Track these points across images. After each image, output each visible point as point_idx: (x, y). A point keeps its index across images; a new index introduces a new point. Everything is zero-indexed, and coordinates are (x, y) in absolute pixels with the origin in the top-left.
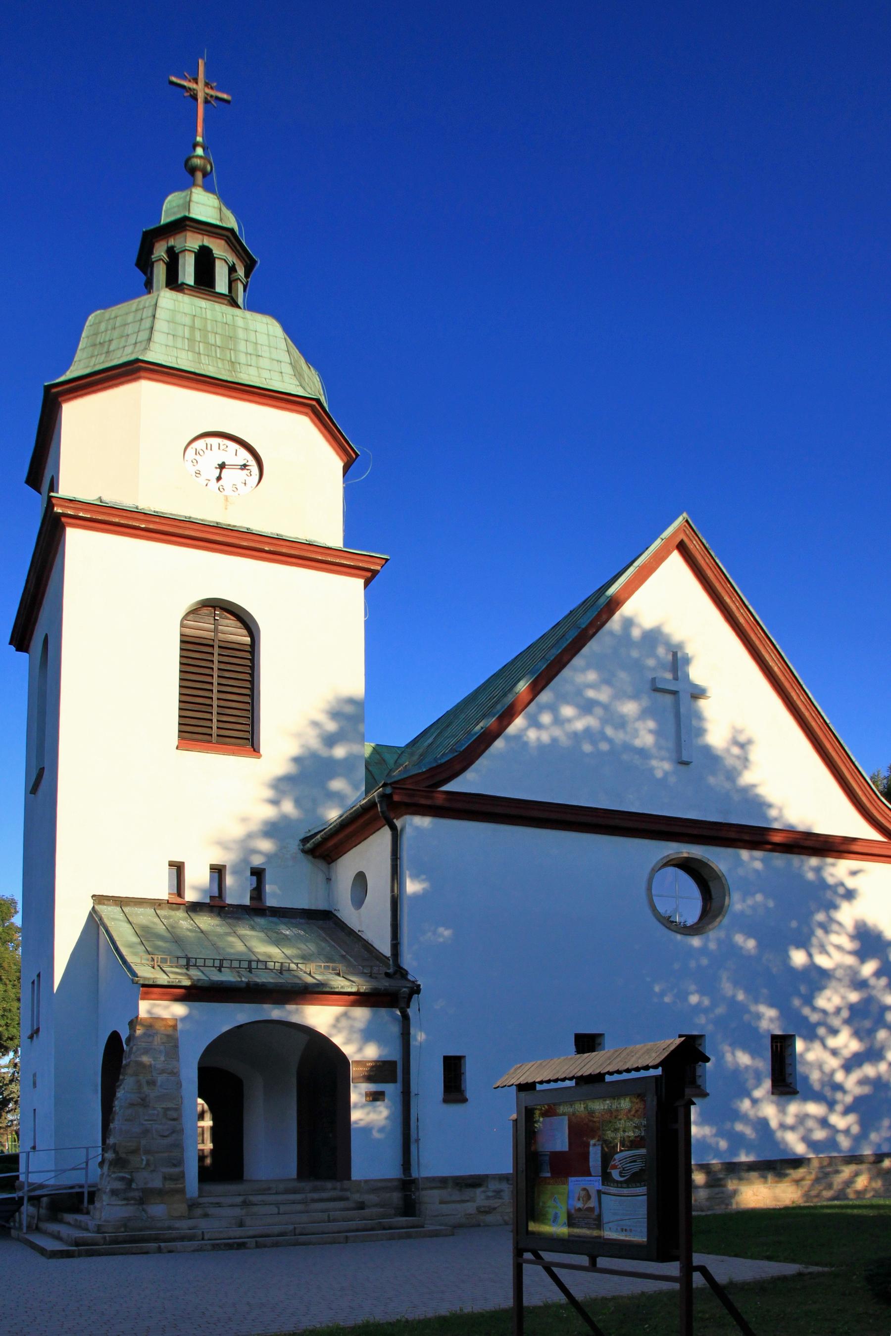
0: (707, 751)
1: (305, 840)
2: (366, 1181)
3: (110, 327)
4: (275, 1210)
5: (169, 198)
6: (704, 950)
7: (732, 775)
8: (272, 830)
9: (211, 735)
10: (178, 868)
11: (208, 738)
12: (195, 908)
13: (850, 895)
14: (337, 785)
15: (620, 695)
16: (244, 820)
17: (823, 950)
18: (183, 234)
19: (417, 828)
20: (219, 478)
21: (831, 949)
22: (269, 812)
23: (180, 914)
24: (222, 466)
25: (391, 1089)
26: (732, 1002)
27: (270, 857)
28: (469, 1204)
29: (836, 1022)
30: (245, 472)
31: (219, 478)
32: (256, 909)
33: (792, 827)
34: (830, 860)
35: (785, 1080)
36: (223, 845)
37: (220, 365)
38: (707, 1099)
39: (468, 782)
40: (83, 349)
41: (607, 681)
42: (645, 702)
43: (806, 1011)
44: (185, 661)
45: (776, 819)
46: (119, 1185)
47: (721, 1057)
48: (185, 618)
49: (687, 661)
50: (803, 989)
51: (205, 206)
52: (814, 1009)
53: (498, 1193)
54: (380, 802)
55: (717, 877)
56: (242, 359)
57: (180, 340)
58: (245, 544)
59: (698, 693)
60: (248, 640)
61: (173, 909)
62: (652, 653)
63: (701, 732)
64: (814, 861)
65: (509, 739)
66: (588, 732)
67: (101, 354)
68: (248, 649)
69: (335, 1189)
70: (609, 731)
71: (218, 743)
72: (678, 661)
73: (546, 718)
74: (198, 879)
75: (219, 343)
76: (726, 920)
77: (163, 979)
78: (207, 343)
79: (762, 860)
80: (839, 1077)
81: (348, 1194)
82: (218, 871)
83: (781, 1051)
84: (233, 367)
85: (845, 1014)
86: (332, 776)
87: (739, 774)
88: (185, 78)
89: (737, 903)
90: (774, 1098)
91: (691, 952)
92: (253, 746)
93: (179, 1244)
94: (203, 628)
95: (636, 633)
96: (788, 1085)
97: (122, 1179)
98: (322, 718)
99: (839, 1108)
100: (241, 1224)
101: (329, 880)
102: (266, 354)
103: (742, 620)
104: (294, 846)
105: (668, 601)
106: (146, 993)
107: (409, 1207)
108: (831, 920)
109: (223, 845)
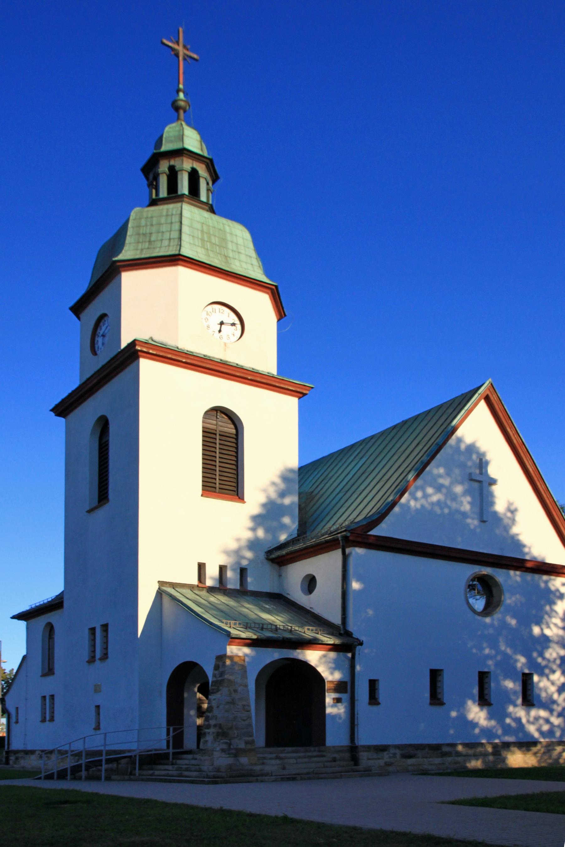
0: (495, 513)
1: (269, 552)
2: (334, 747)
3: (148, 223)
4: (295, 761)
5: (167, 129)
6: (492, 625)
7: (507, 529)
8: (253, 545)
9: (215, 488)
10: (201, 567)
11: (214, 489)
12: (211, 590)
13: (561, 596)
14: (286, 520)
15: (455, 482)
16: (238, 540)
17: (548, 627)
18: (181, 158)
19: (357, 553)
20: (220, 331)
21: (552, 626)
22: (248, 535)
23: (204, 593)
24: (222, 323)
25: (345, 697)
26: (505, 654)
27: (251, 561)
28: (381, 761)
29: (554, 667)
30: (234, 327)
31: (220, 331)
32: (242, 593)
33: (535, 558)
34: (553, 577)
35: (529, 698)
36: (227, 553)
37: (220, 258)
38: (379, 706)
39: (382, 530)
40: (131, 236)
41: (448, 474)
42: (466, 486)
43: (540, 660)
44: (206, 443)
45: (527, 554)
46: (225, 746)
47: (498, 683)
48: (205, 417)
49: (487, 463)
50: (539, 648)
51: (192, 140)
52: (544, 658)
53: (395, 754)
54: (342, 540)
55: (497, 584)
56: (231, 254)
57: (196, 239)
58: (238, 374)
59: (493, 482)
60: (234, 431)
61: (200, 590)
62: (470, 459)
63: (492, 503)
64: (545, 577)
65: (403, 506)
66: (439, 503)
67: (145, 242)
68: (235, 437)
69: (315, 751)
70: (449, 503)
71: (219, 493)
72: (483, 464)
73: (419, 494)
74: (212, 572)
75: (217, 243)
76: (501, 609)
77: (243, 635)
78: (211, 242)
79: (521, 576)
80: (555, 696)
81: (324, 753)
82: (222, 569)
83: (526, 681)
84: (226, 259)
85: (558, 662)
86: (283, 515)
87: (511, 528)
88: (171, 41)
89: (509, 600)
90: (524, 707)
91: (486, 626)
92: (237, 495)
93: (266, 778)
94: (212, 424)
95: (463, 447)
96: (439, 699)
97: (226, 743)
98: (278, 480)
99: (555, 713)
100: (284, 769)
101: (280, 576)
102: (243, 252)
103: (515, 441)
104: (262, 556)
105: (478, 428)
106: (231, 642)
107: (355, 760)
108: (552, 610)
109: (227, 553)
